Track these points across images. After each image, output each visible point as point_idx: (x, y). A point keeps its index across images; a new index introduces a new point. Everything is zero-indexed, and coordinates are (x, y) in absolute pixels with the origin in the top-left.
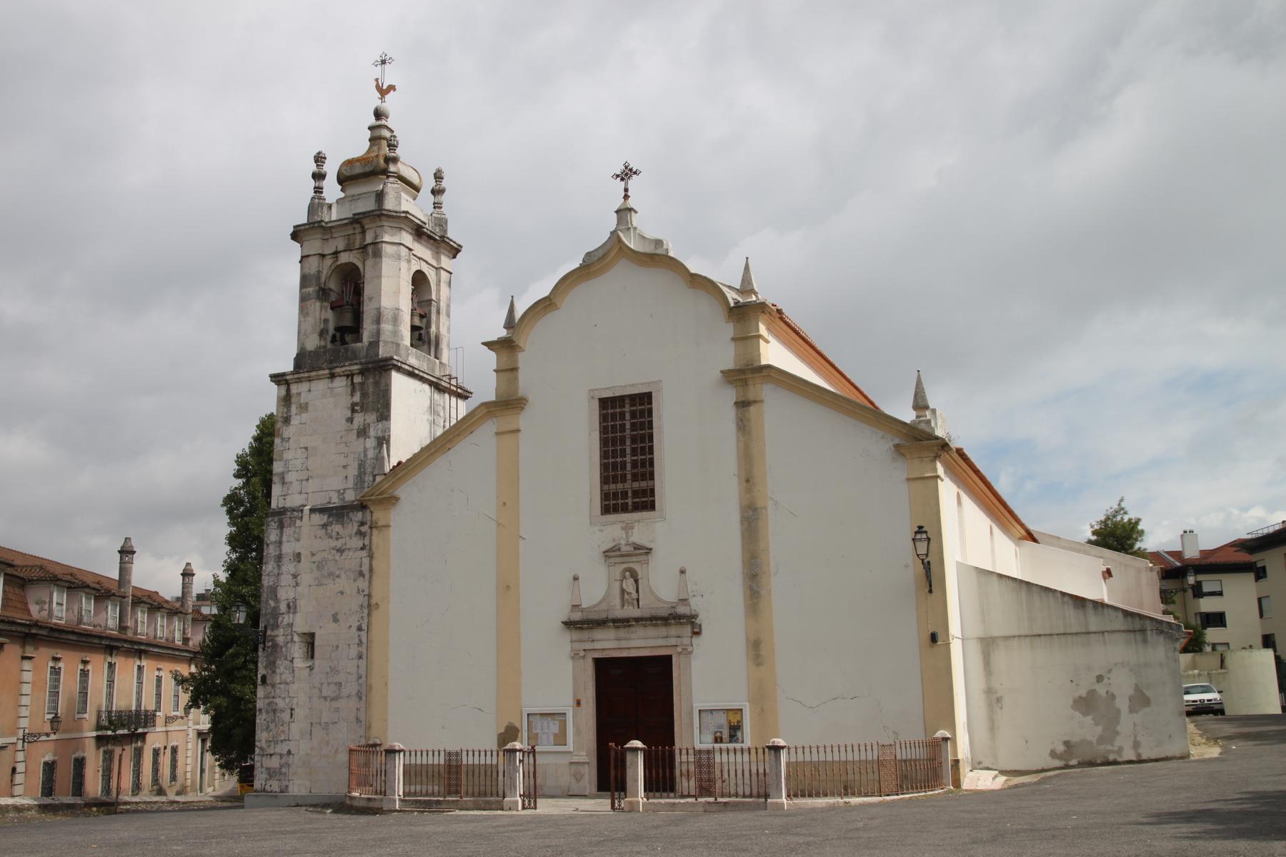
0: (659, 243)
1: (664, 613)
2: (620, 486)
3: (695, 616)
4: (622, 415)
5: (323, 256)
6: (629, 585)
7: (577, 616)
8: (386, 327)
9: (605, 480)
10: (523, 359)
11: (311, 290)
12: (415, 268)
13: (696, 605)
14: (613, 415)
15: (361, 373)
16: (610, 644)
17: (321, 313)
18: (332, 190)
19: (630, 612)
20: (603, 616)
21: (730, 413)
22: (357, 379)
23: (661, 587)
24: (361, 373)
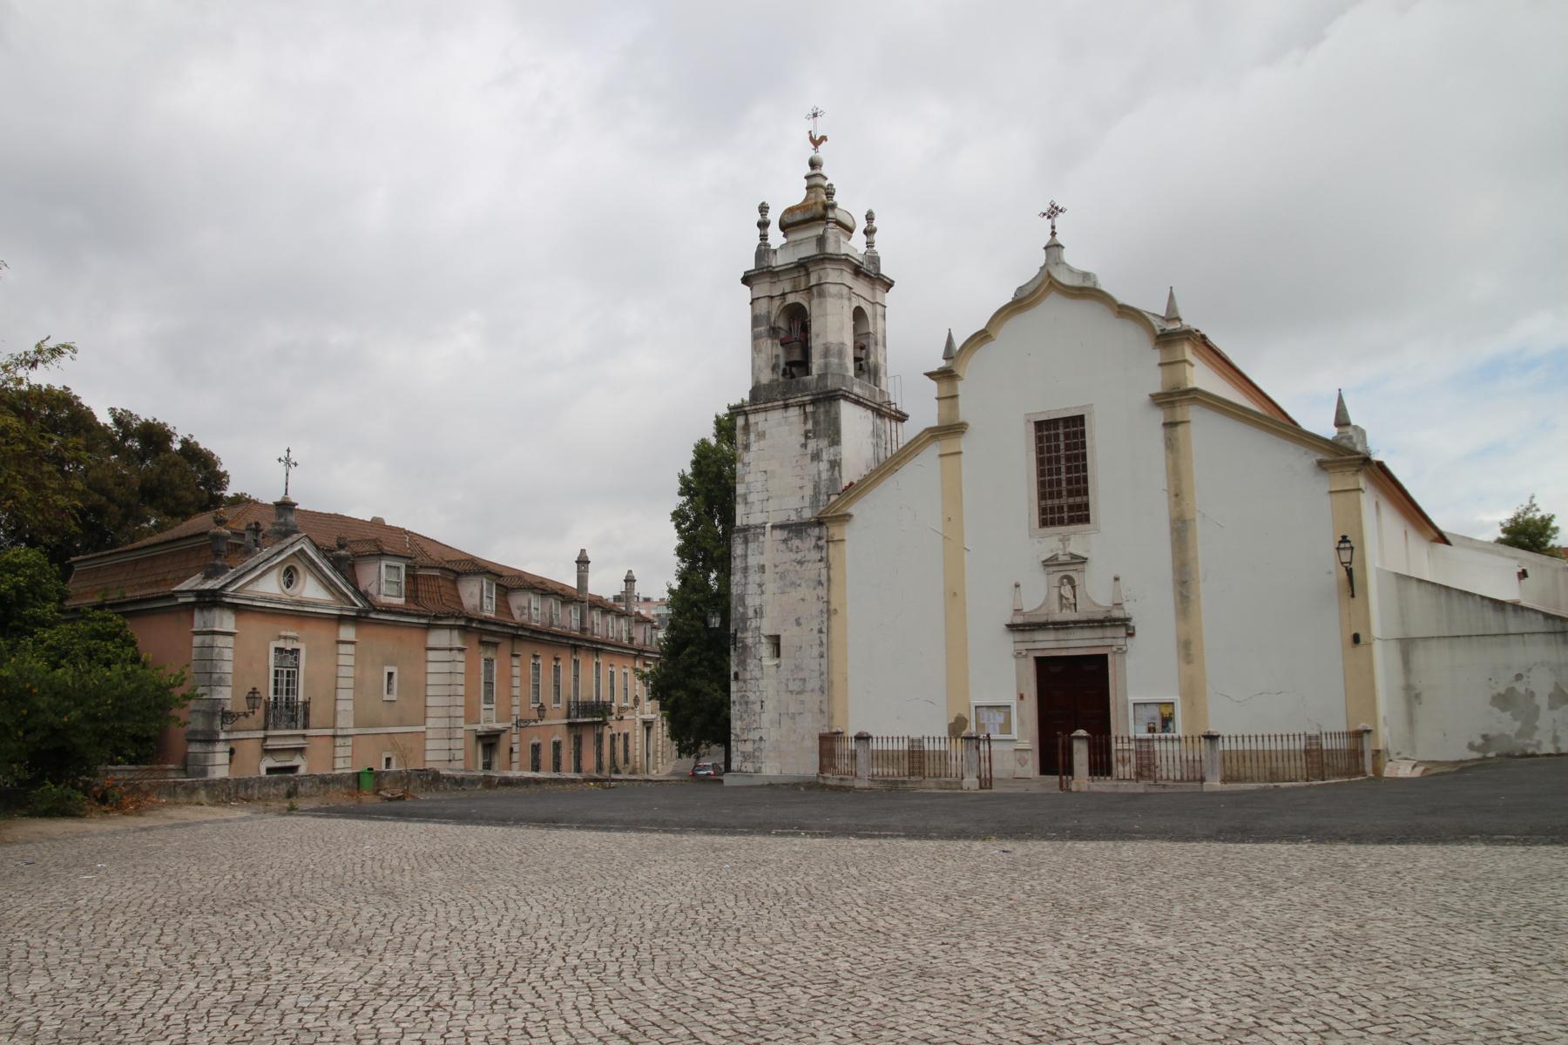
0: (1086, 275)
1: (1100, 617)
2: (1056, 502)
3: (1129, 619)
4: (1057, 436)
5: (772, 297)
6: (1067, 591)
7: (1019, 620)
8: (834, 361)
9: (1042, 496)
10: (961, 387)
12: (855, 304)
13: (1129, 609)
14: (1048, 437)
15: (813, 402)
16: (1049, 643)
17: (772, 349)
18: (776, 238)
19: (1068, 615)
20: (1043, 619)
21: (1159, 434)
22: (809, 409)
23: (1096, 594)
24: (813, 402)
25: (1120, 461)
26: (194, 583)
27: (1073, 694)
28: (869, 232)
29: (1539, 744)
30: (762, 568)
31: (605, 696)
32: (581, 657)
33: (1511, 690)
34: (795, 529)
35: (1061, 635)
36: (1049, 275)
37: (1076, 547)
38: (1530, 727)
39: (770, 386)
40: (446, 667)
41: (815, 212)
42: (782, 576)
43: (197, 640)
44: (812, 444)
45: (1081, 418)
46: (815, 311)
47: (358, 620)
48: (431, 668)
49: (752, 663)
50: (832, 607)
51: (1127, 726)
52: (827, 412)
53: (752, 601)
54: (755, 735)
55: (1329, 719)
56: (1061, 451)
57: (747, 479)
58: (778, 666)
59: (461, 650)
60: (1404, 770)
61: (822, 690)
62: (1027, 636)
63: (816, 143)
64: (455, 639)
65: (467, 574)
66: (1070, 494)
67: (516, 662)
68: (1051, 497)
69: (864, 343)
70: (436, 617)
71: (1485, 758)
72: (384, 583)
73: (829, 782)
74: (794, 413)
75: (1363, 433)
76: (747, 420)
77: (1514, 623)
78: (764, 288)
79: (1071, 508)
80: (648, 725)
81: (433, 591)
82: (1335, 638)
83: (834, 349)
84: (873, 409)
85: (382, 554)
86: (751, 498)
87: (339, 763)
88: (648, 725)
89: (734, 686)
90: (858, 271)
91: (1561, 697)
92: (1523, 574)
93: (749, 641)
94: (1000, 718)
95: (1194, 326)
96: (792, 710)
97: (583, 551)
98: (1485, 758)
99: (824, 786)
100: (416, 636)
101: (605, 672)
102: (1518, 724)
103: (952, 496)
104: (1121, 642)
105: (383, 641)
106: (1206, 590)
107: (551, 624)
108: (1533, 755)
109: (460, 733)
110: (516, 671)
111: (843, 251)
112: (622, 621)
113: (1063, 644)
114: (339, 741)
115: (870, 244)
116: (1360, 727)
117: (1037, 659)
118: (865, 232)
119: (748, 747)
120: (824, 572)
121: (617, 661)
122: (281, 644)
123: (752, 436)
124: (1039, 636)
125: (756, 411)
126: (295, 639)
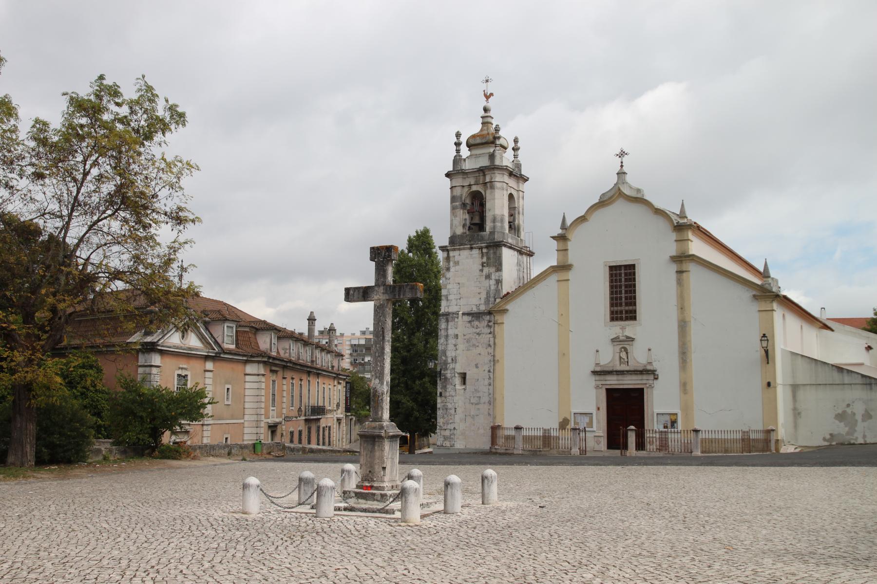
0: (639, 191)
1: (641, 369)
2: (619, 308)
4: (620, 275)
6: (624, 355)
7: (598, 369)
8: (498, 224)
9: (612, 305)
10: (570, 245)
11: (457, 204)
13: (656, 366)
15: (487, 247)
16: (614, 382)
17: (463, 216)
18: (465, 152)
19: (624, 367)
20: (611, 369)
21: (673, 276)
22: (485, 250)
23: (639, 357)
25: (654, 289)
26: (136, 338)
27: (625, 409)
28: (515, 149)
29: (857, 438)
30: (456, 336)
31: (320, 404)
32: (311, 379)
33: (844, 412)
34: (476, 316)
35: (620, 377)
36: (619, 189)
37: (628, 333)
38: (852, 431)
39: (462, 236)
40: (255, 385)
41: (486, 140)
42: (468, 341)
43: (140, 370)
44: (486, 270)
45: (634, 266)
46: (488, 195)
47: (215, 358)
48: (248, 385)
49: (450, 388)
50: (496, 359)
51: (653, 425)
52: (495, 253)
53: (450, 354)
54: (451, 426)
55: (755, 424)
56: (623, 286)
57: (448, 287)
58: (465, 389)
59: (263, 375)
60: (791, 449)
61: (490, 403)
62: (602, 377)
63: (488, 97)
64: (261, 370)
65: (262, 330)
66: (627, 304)
67: (285, 382)
68: (617, 306)
69: (513, 212)
70: (252, 356)
71: (831, 445)
72: (226, 335)
73: (499, 451)
74: (476, 252)
75: (777, 281)
76: (448, 254)
77: (847, 379)
78: (458, 181)
79: (627, 312)
80: (339, 420)
81: (250, 343)
82: (758, 384)
83: (498, 218)
84: (518, 251)
85: (226, 320)
86: (450, 297)
87: (246, 437)
88: (339, 420)
89: (439, 400)
90: (511, 174)
91: (867, 416)
92: (869, 348)
93: (449, 376)
94: (587, 419)
95: (694, 220)
96: (472, 413)
97: (312, 313)
98: (831, 445)
99: (496, 453)
100: (239, 367)
101: (321, 386)
102: (847, 429)
103: (564, 302)
104: (651, 382)
105: (226, 369)
106: (695, 357)
107: (299, 359)
108: (854, 444)
109: (262, 424)
110: (285, 387)
111: (504, 164)
112: (329, 355)
113: (621, 382)
114: (205, 428)
115: (516, 156)
116: (770, 428)
117: (607, 390)
118: (513, 149)
119: (447, 433)
120: (492, 339)
121: (327, 381)
122: (180, 372)
123: (451, 264)
124: (608, 377)
125: (454, 250)
126: (186, 369)
